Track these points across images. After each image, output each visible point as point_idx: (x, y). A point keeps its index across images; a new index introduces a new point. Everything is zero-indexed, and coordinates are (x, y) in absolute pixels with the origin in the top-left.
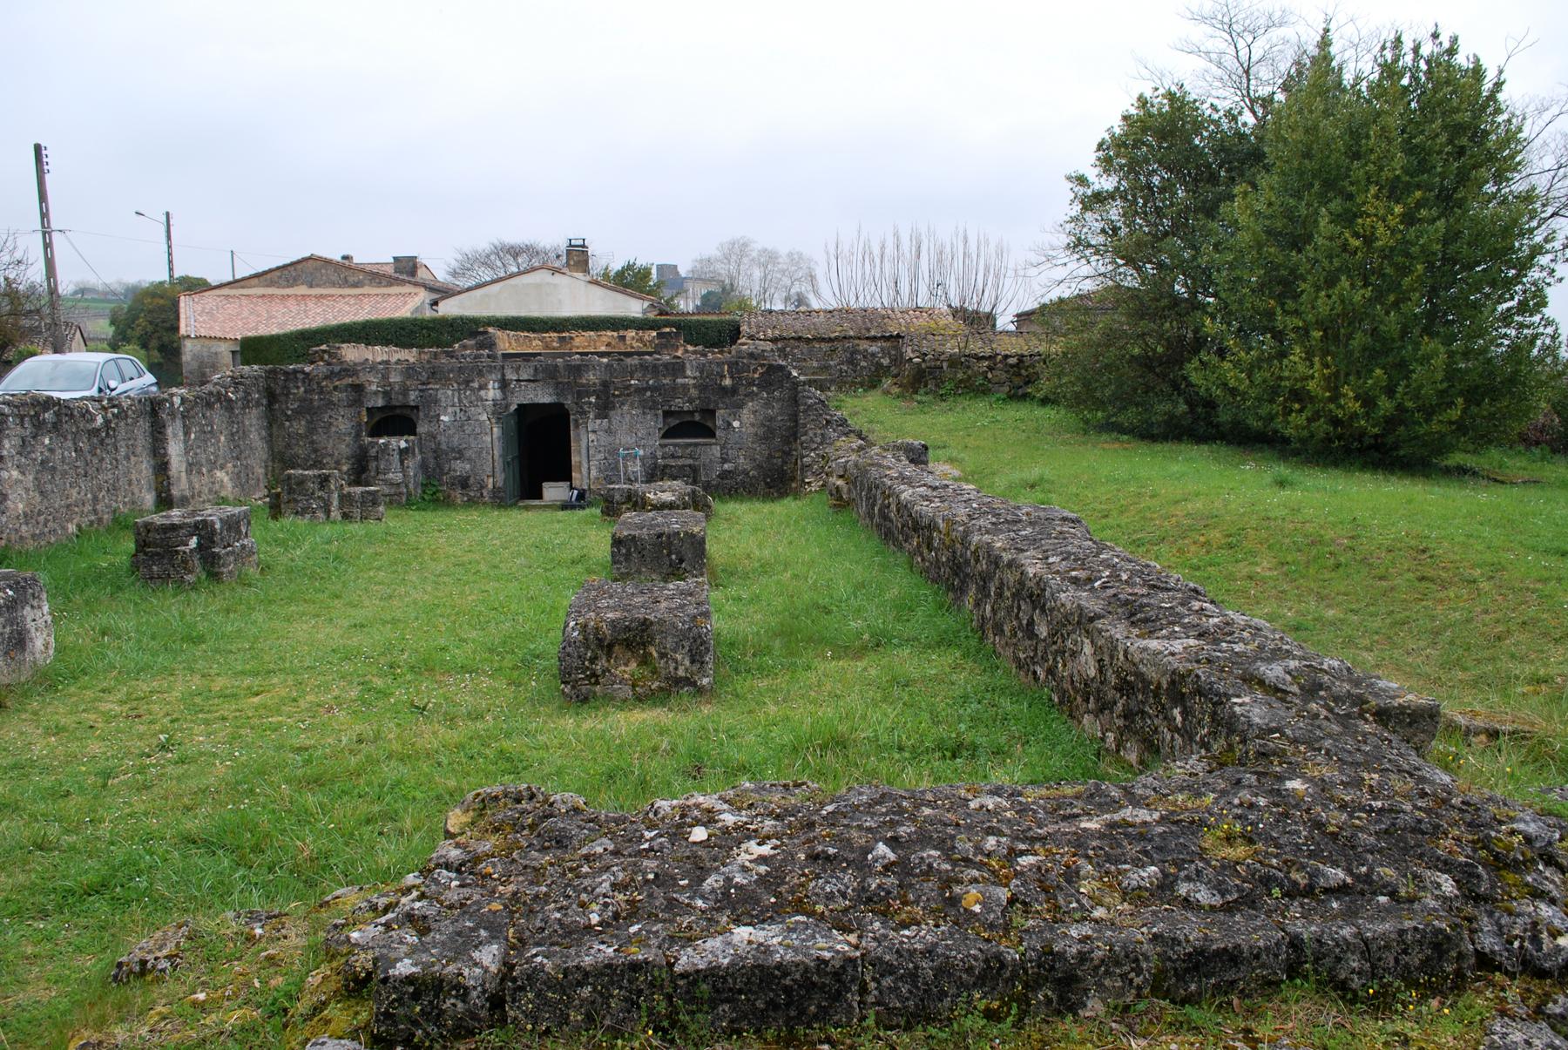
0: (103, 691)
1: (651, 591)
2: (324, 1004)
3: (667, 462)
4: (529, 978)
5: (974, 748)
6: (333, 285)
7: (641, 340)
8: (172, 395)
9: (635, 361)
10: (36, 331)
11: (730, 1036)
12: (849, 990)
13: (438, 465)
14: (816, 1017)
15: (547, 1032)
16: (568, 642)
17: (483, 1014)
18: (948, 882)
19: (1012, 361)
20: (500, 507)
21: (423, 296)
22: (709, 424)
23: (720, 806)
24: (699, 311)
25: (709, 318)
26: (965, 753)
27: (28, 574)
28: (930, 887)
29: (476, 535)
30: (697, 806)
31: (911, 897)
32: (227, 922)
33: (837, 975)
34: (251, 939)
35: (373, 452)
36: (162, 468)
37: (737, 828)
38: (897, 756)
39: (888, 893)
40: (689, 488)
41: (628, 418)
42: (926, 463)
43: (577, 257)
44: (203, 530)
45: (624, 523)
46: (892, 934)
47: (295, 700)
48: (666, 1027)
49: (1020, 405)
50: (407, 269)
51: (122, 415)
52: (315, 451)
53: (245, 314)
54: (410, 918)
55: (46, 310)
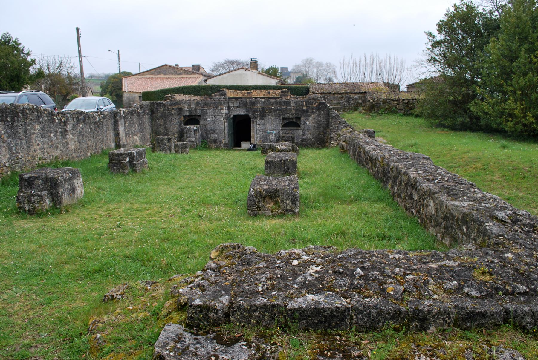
1: (278, 179)
2: (171, 312)
4: (238, 308)
5: (390, 237)
6: (172, 74)
7: (275, 93)
8: (120, 111)
9: (273, 100)
10: (77, 90)
14: (335, 327)
15: (244, 326)
16: (250, 196)
17: (223, 319)
18: (382, 283)
20: (227, 150)
21: (202, 78)
22: (298, 123)
24: (295, 83)
26: (387, 239)
27: (76, 169)
28: (376, 284)
29: (219, 159)
30: (295, 253)
31: (369, 287)
32: (139, 284)
33: (343, 313)
34: (146, 290)
35: (185, 130)
36: (117, 135)
37: (308, 261)
38: (363, 239)
39: (361, 286)
40: (291, 144)
42: (374, 137)
43: (254, 65)
44: (130, 155)
45: (269, 156)
46: (362, 300)
47: (160, 212)
50: (197, 69)
51: (105, 117)
52: (166, 130)
53: (144, 84)
54: (199, 286)
55: (80, 83)
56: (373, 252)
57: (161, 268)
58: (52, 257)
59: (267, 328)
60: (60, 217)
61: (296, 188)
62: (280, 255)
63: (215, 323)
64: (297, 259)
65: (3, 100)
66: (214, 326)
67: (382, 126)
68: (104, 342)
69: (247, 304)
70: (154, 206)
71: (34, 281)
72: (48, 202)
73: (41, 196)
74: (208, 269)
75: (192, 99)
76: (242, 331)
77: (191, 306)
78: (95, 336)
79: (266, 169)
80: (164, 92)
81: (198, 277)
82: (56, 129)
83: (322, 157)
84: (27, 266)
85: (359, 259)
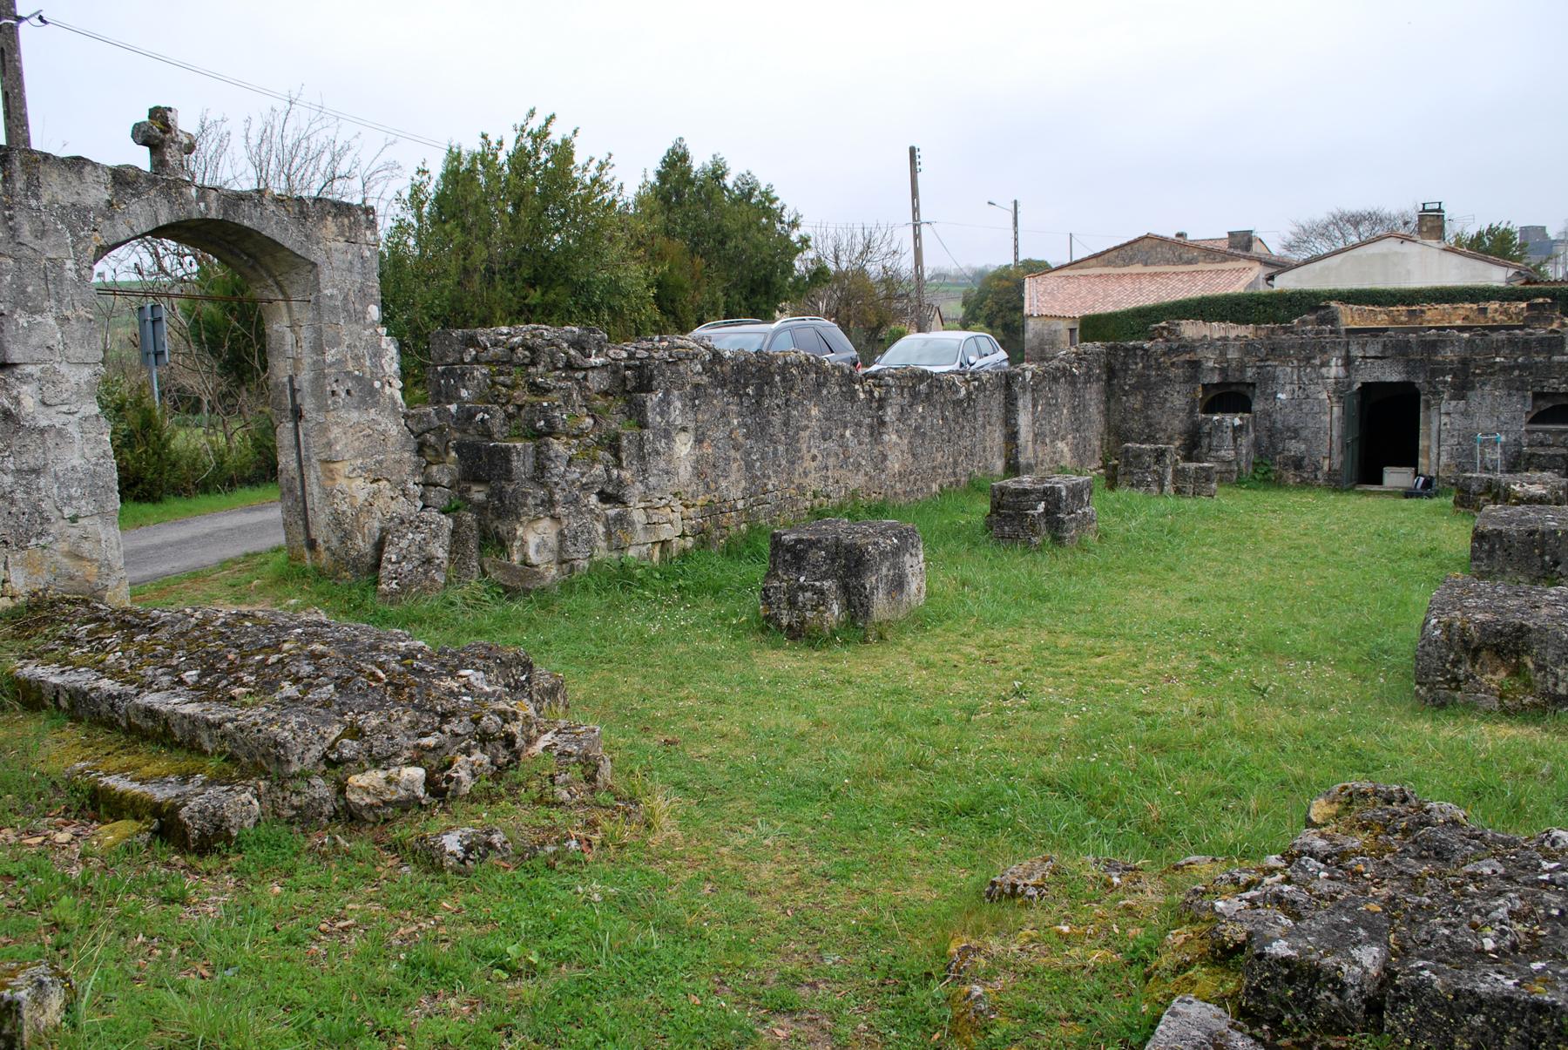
0: (964, 635)
1: (1528, 594)
3: (1534, 450)
4: (1414, 990)
6: (1168, 262)
7: (1505, 312)
8: (1024, 370)
9: (1502, 335)
10: (903, 312)
16: (1426, 639)
17: (1359, 1015)
20: (1335, 490)
21: (1258, 271)
27: (909, 526)
29: (1311, 518)
34: (1108, 885)
35: (1206, 428)
36: (1012, 436)
41: (1489, 400)
43: (1431, 223)
44: (1050, 495)
45: (1487, 516)
47: (1135, 665)
50: (1242, 243)
51: (981, 388)
52: (1149, 425)
53: (1084, 293)
54: (1278, 899)
57: (1144, 828)
58: (848, 754)
60: (865, 652)
62: (1553, 843)
66: (1328, 1031)
68: (993, 1010)
69: (1446, 986)
70: (1115, 645)
71: (809, 812)
72: (835, 607)
73: (821, 592)
75: (1232, 334)
77: (1261, 956)
78: (966, 989)
80: (1143, 320)
81: (1271, 871)
82: (859, 417)
84: (789, 771)
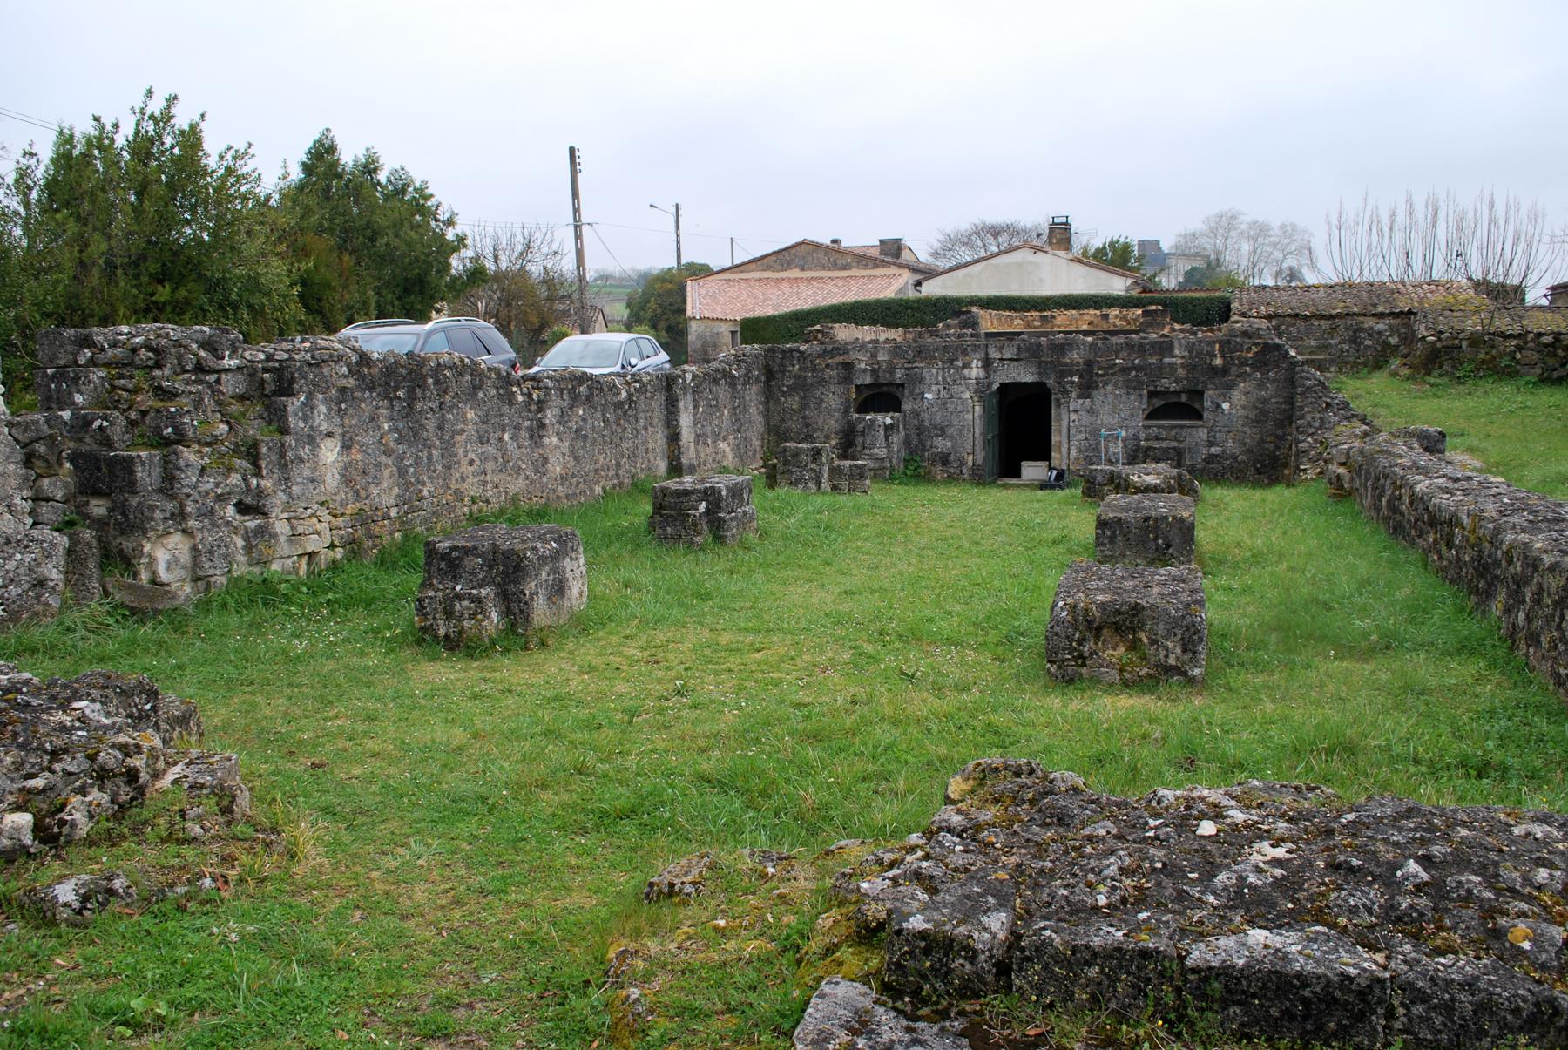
1: (1142, 575)
2: (837, 947)
3: (1150, 443)
4: (1037, 950)
5: (1504, 770)
6: (823, 268)
7: (1124, 318)
9: (1120, 339)
10: (566, 313)
11: (1240, 1040)
12: (1374, 1012)
13: (921, 441)
14: (1334, 1035)
15: (1051, 1006)
17: (990, 978)
18: (1490, 912)
19: (1545, 339)
20: (978, 484)
21: (907, 277)
22: (1197, 406)
23: (1226, 802)
24: (1182, 288)
25: (1197, 295)
26: (1493, 774)
27: (569, 530)
28: (1470, 913)
30: (1203, 799)
31: (1447, 923)
32: (742, 859)
33: (1362, 994)
34: (763, 876)
35: (860, 427)
36: (674, 438)
37: (1247, 826)
38: (1413, 769)
39: (1422, 915)
40: (1175, 472)
41: (1111, 398)
42: (1442, 452)
43: (1060, 235)
44: (711, 495)
45: (1109, 505)
46: (1425, 959)
48: (1177, 1022)
49: (1555, 390)
50: (892, 250)
52: (807, 425)
53: (744, 296)
54: (917, 876)
55: (576, 296)
56: (1454, 811)
57: (799, 817)
59: (1121, 1017)
61: (1196, 602)
62: (1159, 802)
63: (966, 987)
64: (1210, 819)
65: (386, 343)
66: (963, 997)
67: (1468, 418)
68: (651, 1011)
70: (775, 639)
71: (464, 828)
72: (494, 616)
73: (478, 600)
74: (940, 829)
75: (882, 338)
76: (1047, 1022)
77: (899, 932)
79: (1098, 543)
80: (798, 324)
81: (912, 849)
82: (517, 420)
83: (1273, 512)
84: (445, 786)
85: (1411, 830)
